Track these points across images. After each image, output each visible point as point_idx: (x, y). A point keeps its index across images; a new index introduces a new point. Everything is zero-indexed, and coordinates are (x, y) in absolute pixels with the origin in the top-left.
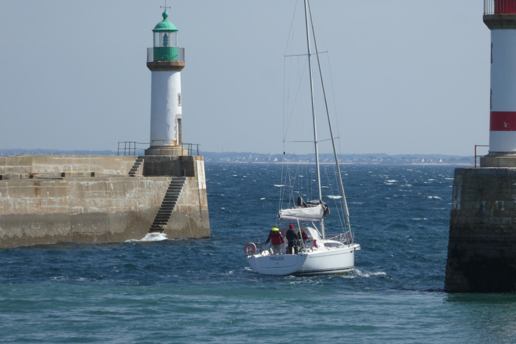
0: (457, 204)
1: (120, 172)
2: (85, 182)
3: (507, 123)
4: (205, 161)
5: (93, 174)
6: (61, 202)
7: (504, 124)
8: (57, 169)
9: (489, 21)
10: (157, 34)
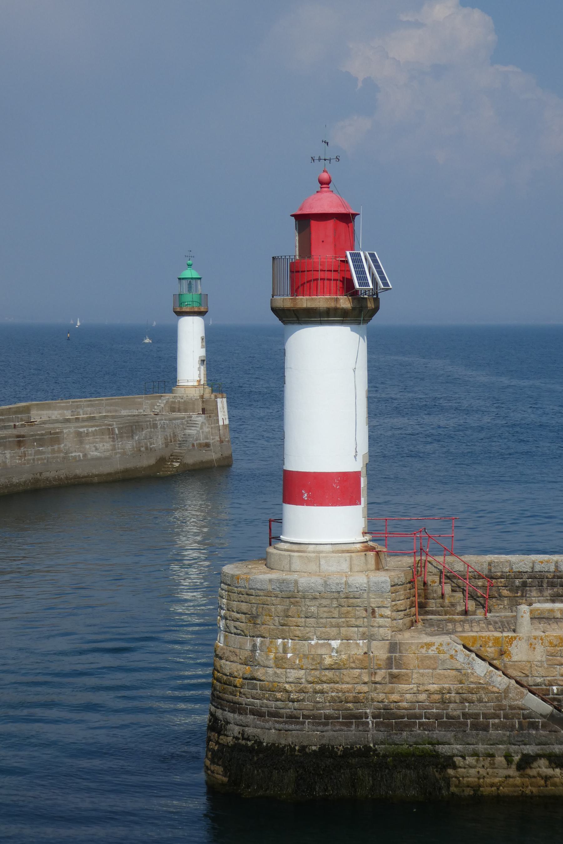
1: (142, 411)
2: (85, 429)
3: (308, 492)
4: (227, 398)
6: (53, 451)
7: (303, 494)
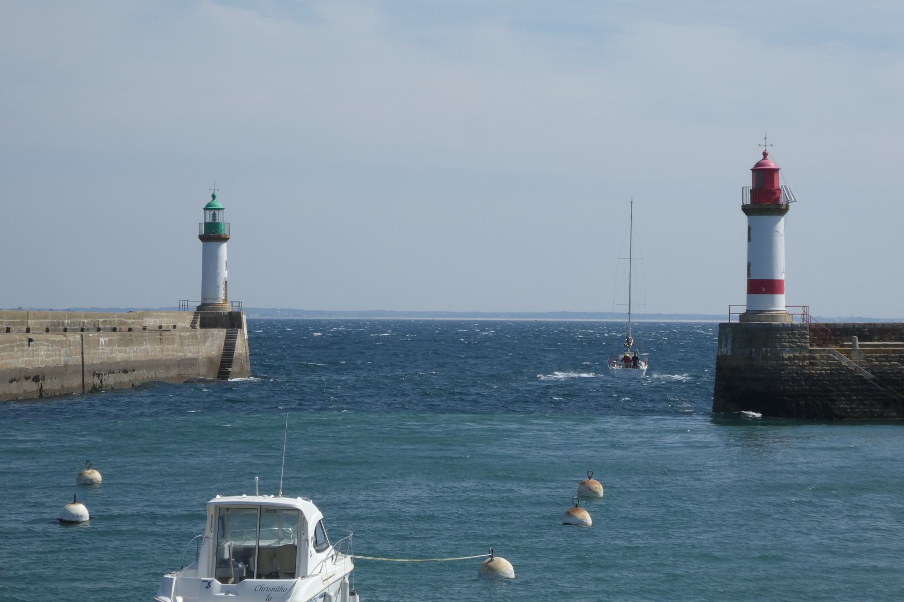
0: (727, 350)
5: (175, 327)
8: (155, 322)
9: (746, 209)
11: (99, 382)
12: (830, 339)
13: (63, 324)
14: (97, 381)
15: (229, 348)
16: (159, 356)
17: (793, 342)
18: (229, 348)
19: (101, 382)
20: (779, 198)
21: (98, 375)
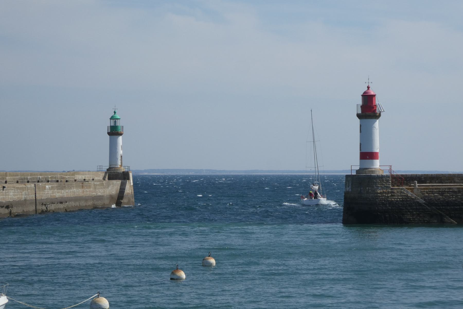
0: (349, 189)
5: (93, 179)
9: (359, 116)
10: (112, 120)
11: (45, 208)
12: (404, 183)
13: (27, 179)
14: (44, 208)
15: (122, 190)
16: (81, 195)
17: (382, 184)
18: (122, 190)
19: (47, 208)
20: (376, 110)
21: (45, 205)
